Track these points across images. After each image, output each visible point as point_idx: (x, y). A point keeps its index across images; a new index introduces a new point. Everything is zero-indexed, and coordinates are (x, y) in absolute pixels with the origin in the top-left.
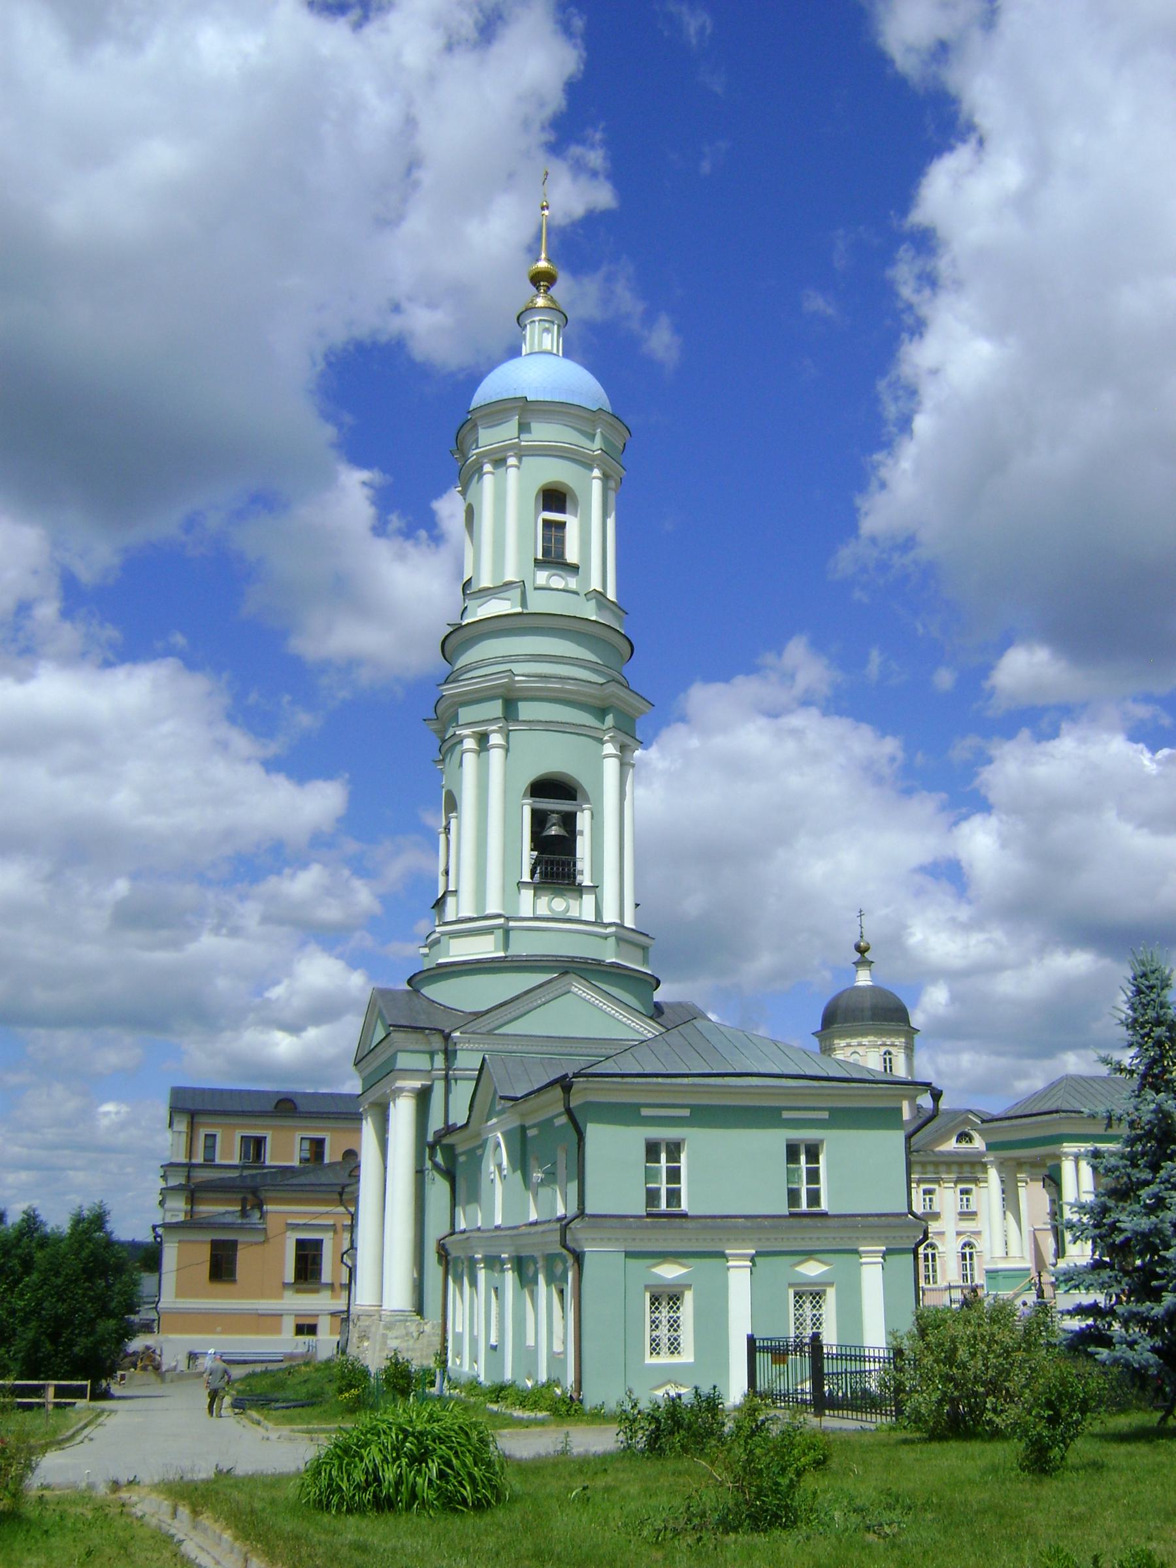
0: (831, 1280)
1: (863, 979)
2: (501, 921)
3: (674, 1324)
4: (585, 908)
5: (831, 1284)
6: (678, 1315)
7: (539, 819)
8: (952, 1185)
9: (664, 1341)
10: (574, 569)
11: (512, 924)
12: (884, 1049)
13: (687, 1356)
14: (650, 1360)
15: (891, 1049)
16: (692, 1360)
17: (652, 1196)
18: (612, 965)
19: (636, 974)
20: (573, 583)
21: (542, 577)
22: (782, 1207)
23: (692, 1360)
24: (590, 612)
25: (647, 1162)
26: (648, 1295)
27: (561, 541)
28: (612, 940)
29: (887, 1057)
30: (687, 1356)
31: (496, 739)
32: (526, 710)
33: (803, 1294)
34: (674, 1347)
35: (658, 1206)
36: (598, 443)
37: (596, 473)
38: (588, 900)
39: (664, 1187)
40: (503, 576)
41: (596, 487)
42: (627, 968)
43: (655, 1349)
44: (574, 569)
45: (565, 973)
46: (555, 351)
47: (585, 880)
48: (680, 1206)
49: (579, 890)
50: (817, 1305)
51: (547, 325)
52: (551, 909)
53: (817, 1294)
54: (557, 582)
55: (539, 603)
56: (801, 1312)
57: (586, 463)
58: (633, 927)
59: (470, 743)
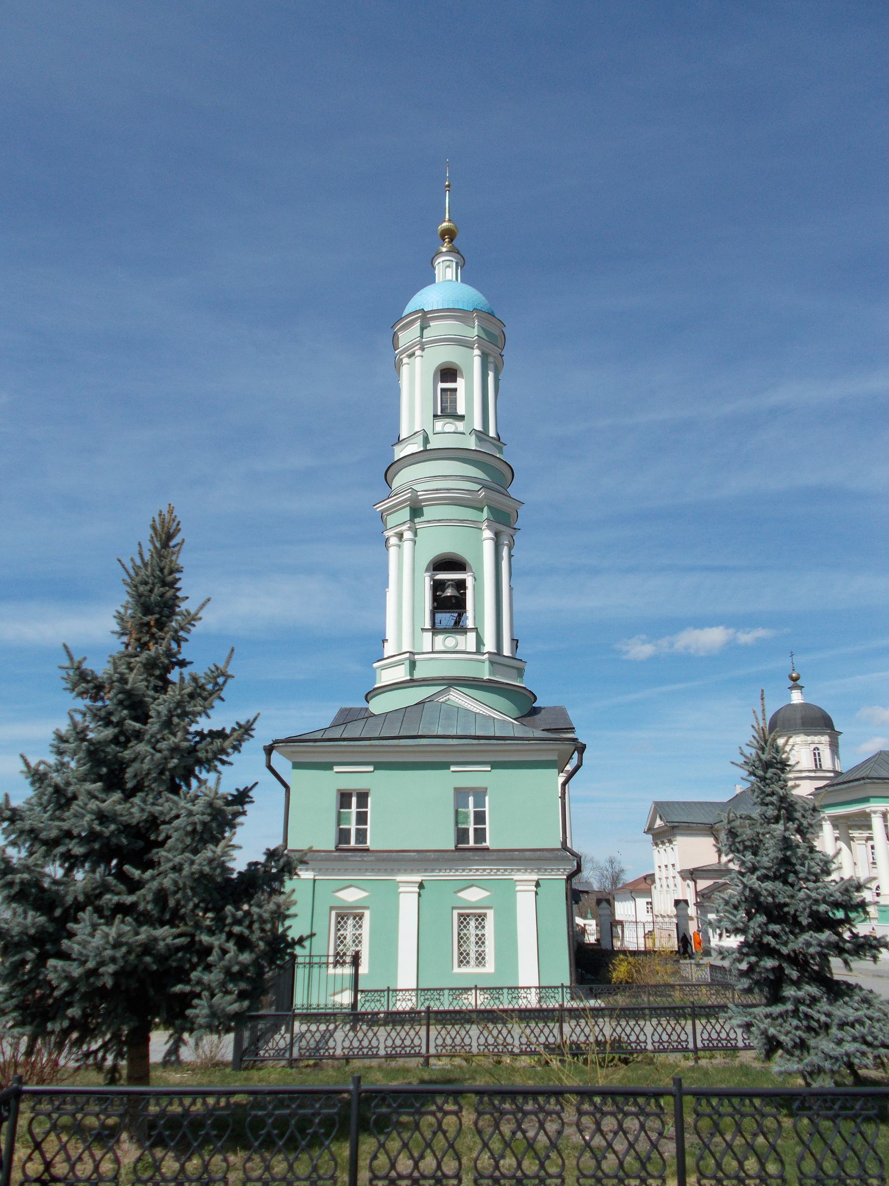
0: (490, 905)
1: (796, 698)
2: (407, 655)
3: (480, 941)
4: (468, 642)
5: (367, 908)
6: (483, 932)
7: (438, 586)
8: (864, 842)
9: (473, 955)
10: (461, 418)
11: (416, 657)
12: (813, 746)
13: (490, 967)
14: (456, 970)
15: (818, 746)
16: (492, 970)
17: (343, 836)
18: (490, 681)
19: (509, 687)
20: (460, 426)
21: (439, 425)
22: (448, 842)
23: (492, 970)
24: (471, 443)
25: (341, 808)
26: (333, 913)
27: (454, 401)
28: (487, 663)
29: (817, 752)
30: (490, 967)
31: (408, 535)
32: (429, 513)
33: (468, 916)
34: (481, 959)
35: (349, 843)
36: (475, 332)
37: (477, 352)
38: (472, 636)
39: (353, 827)
40: (414, 428)
41: (477, 362)
42: (497, 682)
43: (463, 960)
44: (461, 418)
45: (450, 686)
46: (454, 279)
47: (470, 624)
48: (366, 843)
49: (464, 631)
50: (480, 926)
51: (448, 263)
52: (445, 646)
53: (480, 916)
54: (450, 428)
55: (435, 443)
56: (465, 931)
57: (468, 345)
58: (510, 655)
59: (393, 541)
